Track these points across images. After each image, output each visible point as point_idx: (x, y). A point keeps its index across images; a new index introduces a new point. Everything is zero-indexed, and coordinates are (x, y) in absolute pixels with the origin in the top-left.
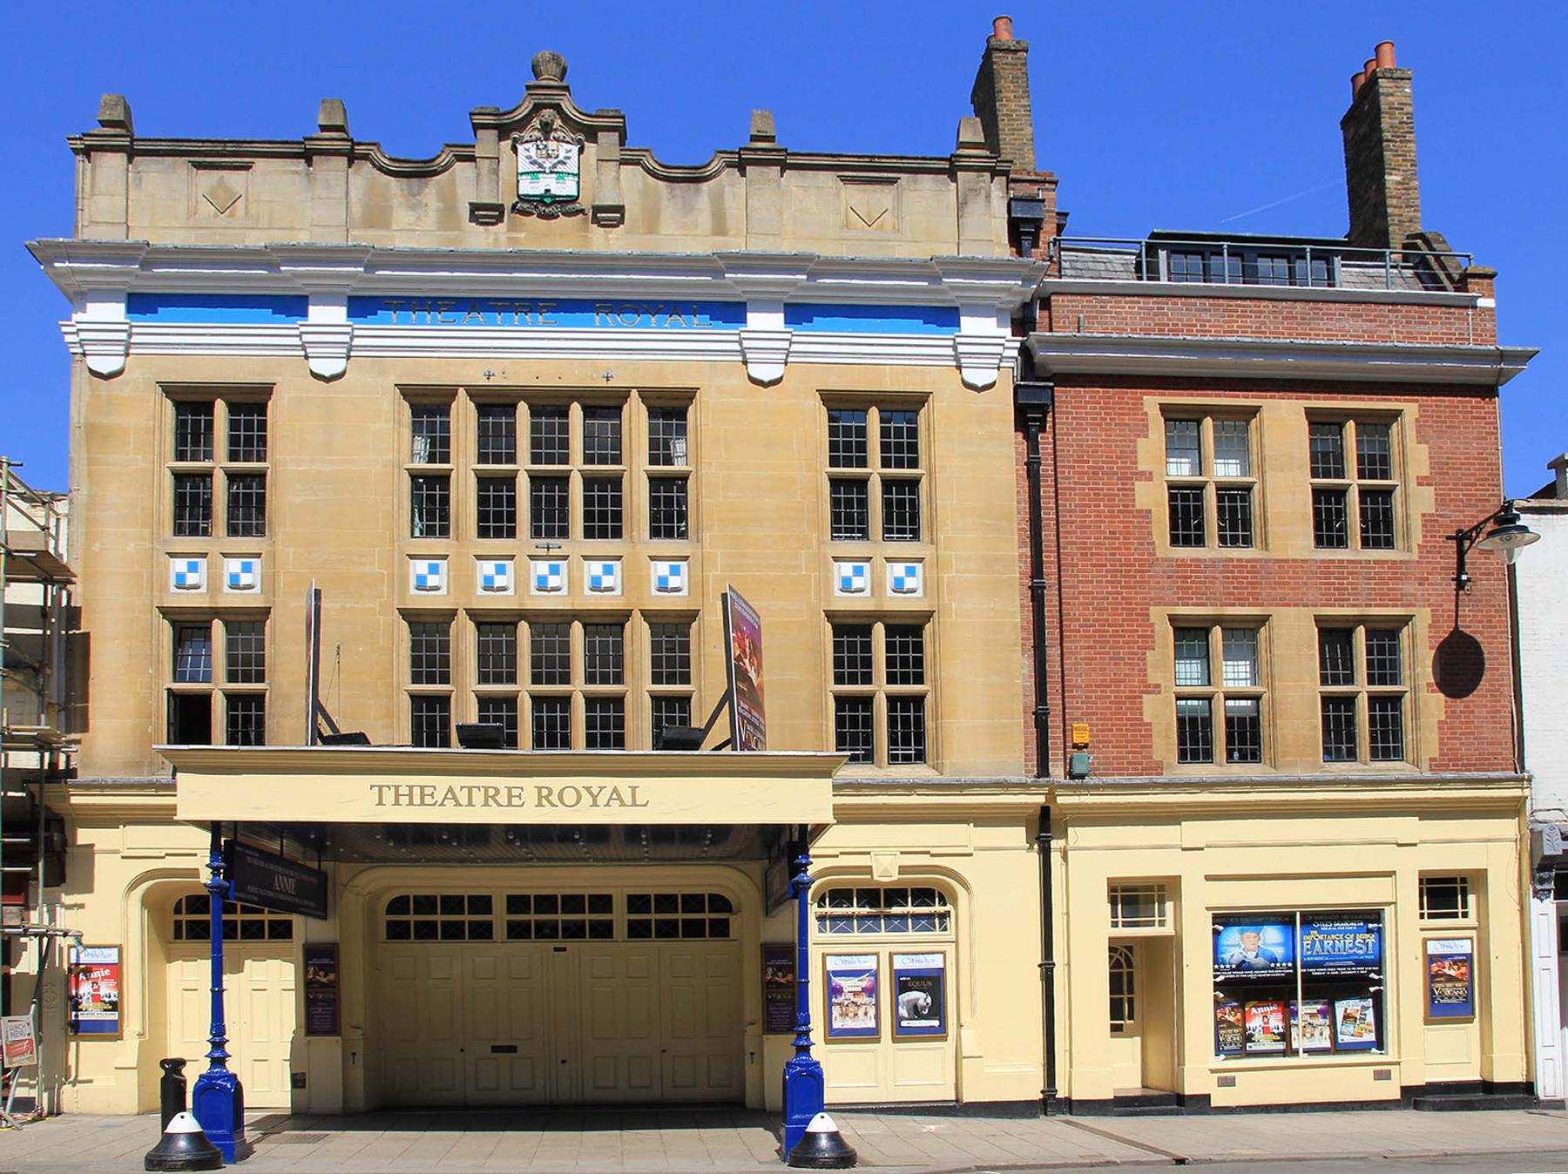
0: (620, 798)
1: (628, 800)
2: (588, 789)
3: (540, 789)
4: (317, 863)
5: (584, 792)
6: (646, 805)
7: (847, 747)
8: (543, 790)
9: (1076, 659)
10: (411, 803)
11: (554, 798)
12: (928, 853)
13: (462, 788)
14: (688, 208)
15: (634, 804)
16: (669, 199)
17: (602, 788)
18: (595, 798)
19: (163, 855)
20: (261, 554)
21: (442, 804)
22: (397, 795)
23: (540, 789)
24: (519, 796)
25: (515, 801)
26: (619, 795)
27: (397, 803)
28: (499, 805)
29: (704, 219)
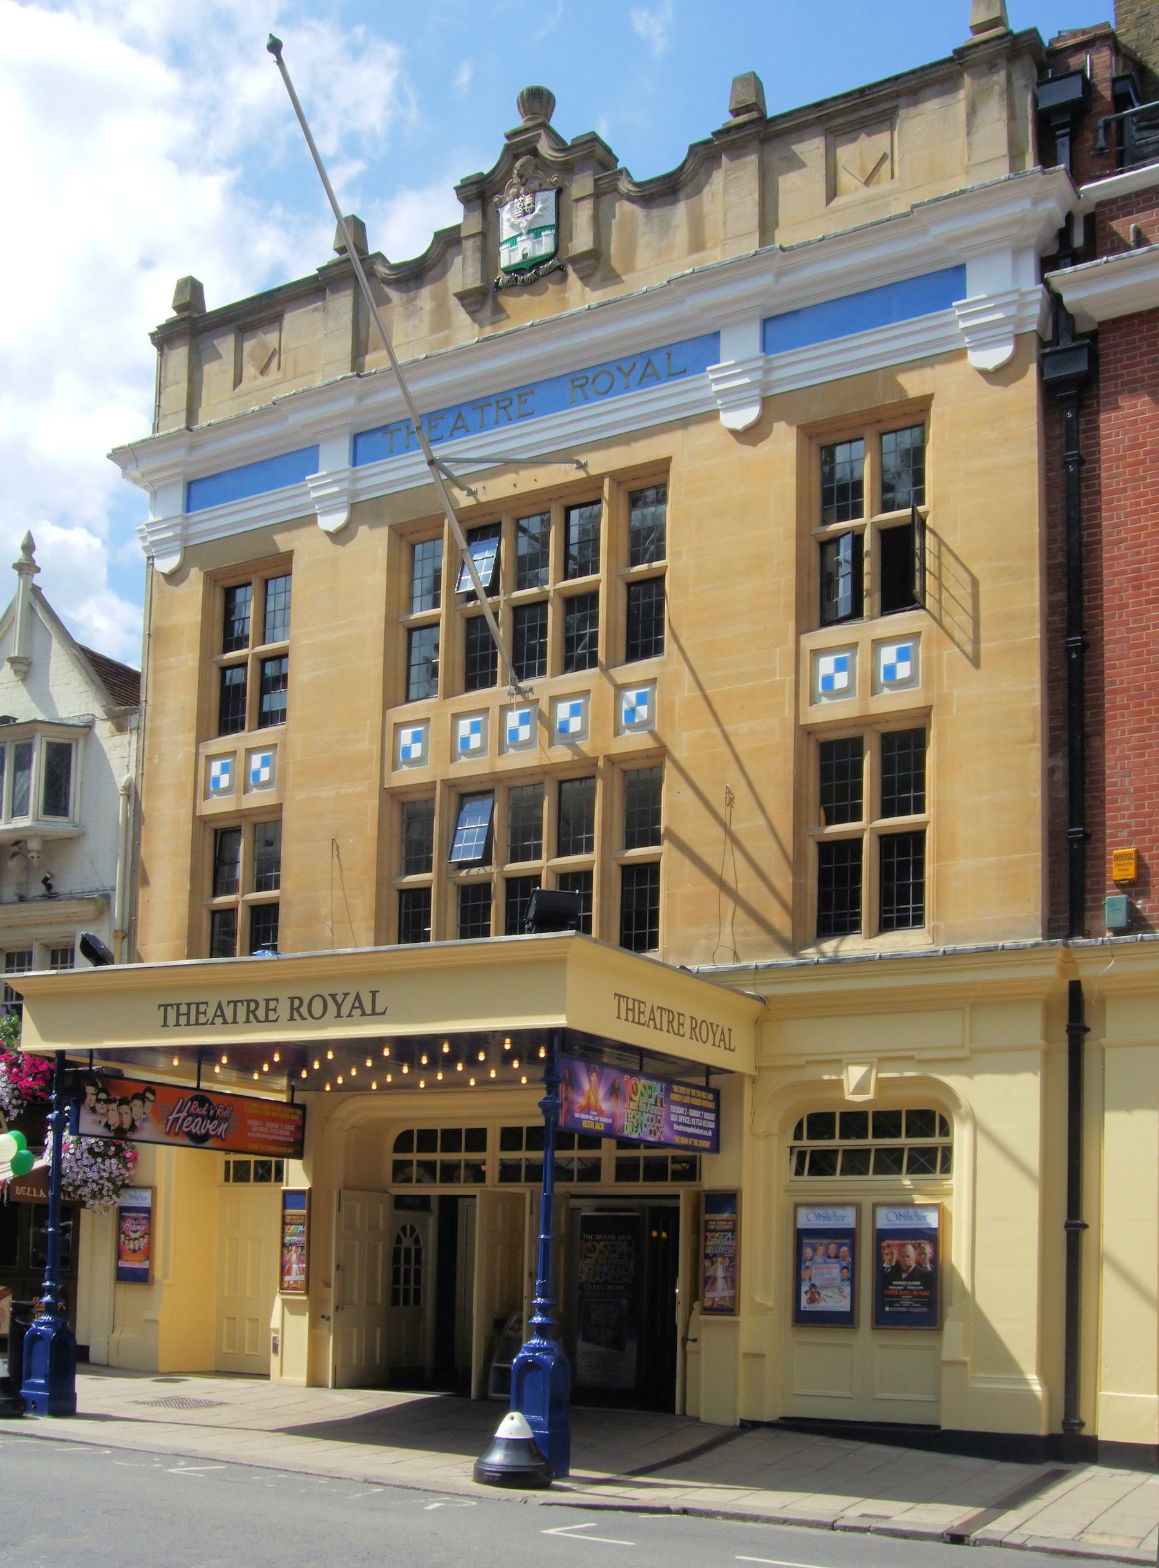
0: (361, 1007)
1: (368, 1010)
2: (333, 996)
3: (292, 999)
4: (704, 1079)
5: (330, 1001)
6: (384, 1013)
7: (15, 968)
8: (271, 1002)
9: (1122, 750)
10: (188, 1024)
11: (304, 1010)
12: (912, 1058)
13: (229, 1002)
14: (665, 229)
15: (374, 1013)
16: (646, 224)
17: (346, 995)
18: (339, 1006)
19: (803, 1063)
20: (487, 709)
21: (213, 1023)
22: (178, 1015)
23: (292, 999)
24: (275, 1010)
25: (272, 1016)
26: (222, 1011)
27: (178, 1024)
28: (258, 1021)
29: (681, 236)
